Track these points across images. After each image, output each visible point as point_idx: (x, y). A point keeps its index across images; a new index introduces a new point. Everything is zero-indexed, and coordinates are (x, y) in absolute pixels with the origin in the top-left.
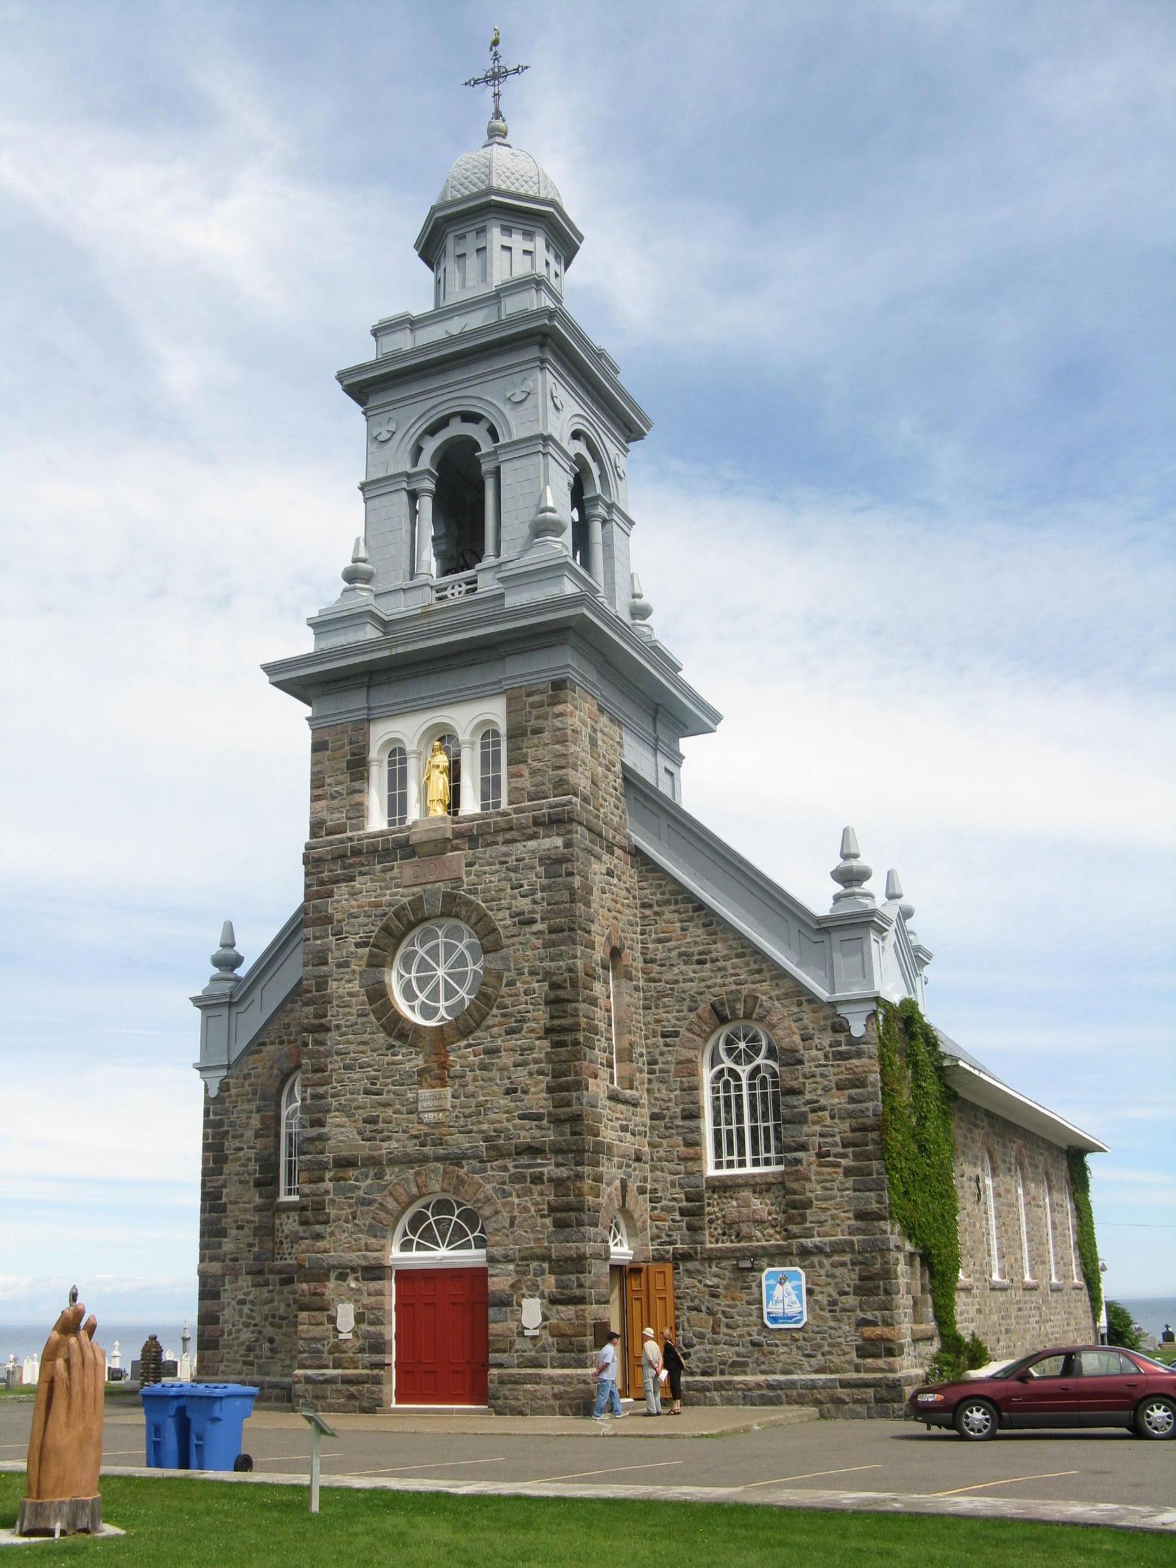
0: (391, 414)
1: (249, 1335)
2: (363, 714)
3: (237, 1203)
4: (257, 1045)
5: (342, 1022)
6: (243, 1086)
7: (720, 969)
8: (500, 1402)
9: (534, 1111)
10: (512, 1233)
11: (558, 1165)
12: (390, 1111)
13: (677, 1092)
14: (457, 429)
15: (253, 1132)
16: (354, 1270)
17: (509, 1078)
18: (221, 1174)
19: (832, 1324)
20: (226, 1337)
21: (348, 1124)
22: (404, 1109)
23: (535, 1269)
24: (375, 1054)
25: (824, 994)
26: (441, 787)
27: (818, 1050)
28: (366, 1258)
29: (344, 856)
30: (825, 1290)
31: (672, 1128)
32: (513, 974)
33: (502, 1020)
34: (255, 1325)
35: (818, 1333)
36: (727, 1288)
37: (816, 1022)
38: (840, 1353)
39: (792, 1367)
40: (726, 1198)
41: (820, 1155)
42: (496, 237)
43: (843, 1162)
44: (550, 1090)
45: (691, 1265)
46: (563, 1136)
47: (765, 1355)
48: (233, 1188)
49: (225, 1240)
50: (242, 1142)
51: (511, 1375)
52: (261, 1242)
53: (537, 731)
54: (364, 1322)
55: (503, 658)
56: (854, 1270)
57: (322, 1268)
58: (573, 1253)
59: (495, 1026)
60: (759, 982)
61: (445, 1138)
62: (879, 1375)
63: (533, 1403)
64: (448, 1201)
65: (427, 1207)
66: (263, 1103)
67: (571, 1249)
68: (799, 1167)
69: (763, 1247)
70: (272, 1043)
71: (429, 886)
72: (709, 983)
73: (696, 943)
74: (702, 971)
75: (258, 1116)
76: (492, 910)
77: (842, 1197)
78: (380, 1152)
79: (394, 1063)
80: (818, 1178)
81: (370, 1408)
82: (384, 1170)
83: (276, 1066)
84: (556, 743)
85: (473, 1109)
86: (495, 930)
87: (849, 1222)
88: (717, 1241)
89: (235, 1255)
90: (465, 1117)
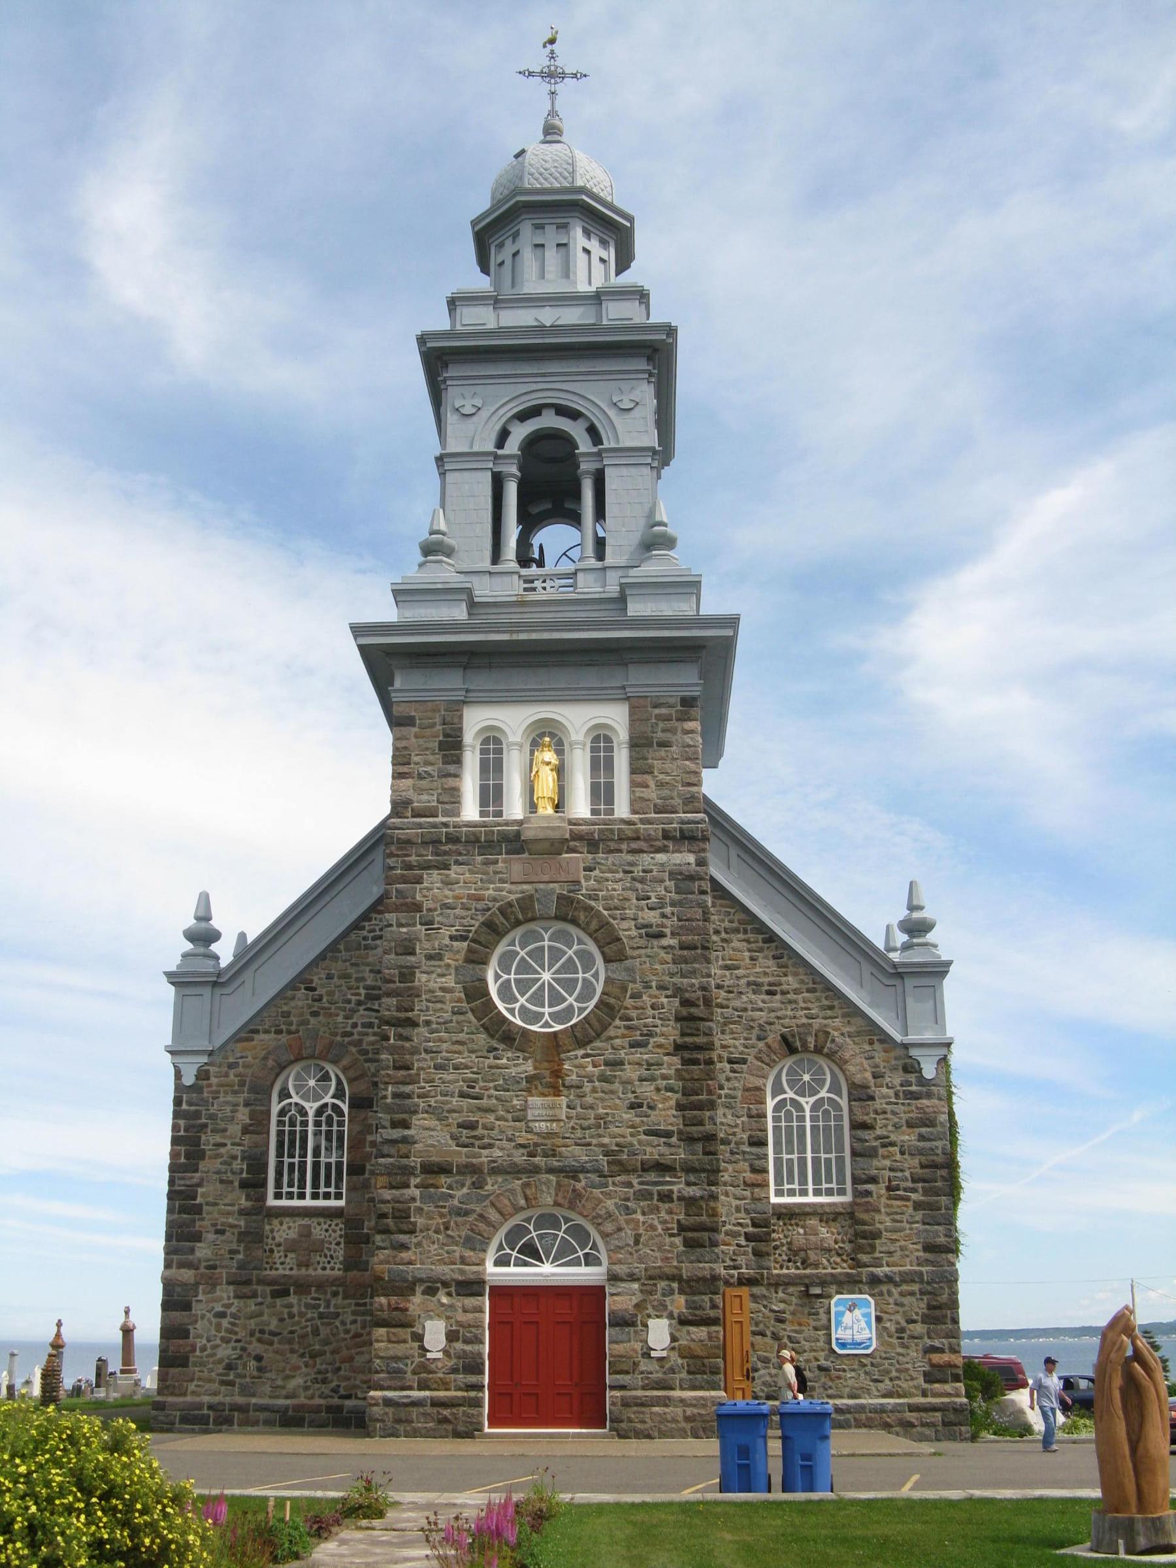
0: (478, 389)
1: (229, 1352)
2: (459, 696)
3: (216, 1204)
4: (248, 1032)
5: (433, 1019)
6: (226, 1075)
7: (790, 1002)
8: (623, 1425)
9: (662, 1128)
10: (637, 1251)
11: (688, 1184)
12: (491, 1118)
13: (745, 1119)
14: (549, 420)
15: (240, 1127)
16: (445, 1284)
17: (634, 1092)
18: (196, 1171)
19: (900, 1350)
20: (198, 1353)
21: (439, 1128)
22: (509, 1116)
23: (663, 1289)
24: (473, 1056)
25: (898, 1037)
26: (551, 784)
27: (888, 1087)
28: (462, 1272)
29: (436, 842)
30: (892, 1317)
31: (738, 1154)
32: (639, 986)
33: (626, 1032)
34: (238, 1341)
35: (887, 1358)
36: (793, 1313)
37: (888, 1062)
38: (908, 1378)
39: (859, 1392)
40: (791, 1225)
41: (889, 1189)
42: (578, 238)
43: (913, 1196)
44: (680, 1107)
45: (757, 1290)
46: (697, 1156)
47: (832, 1380)
48: (211, 1188)
49: (199, 1245)
50: (224, 1138)
51: (636, 1398)
52: (247, 1249)
53: (664, 744)
54: (457, 1340)
55: (626, 665)
56: (922, 1300)
57: (406, 1281)
58: (707, 1274)
59: (617, 1037)
60: (831, 1018)
61: (558, 1149)
62: (946, 1400)
63: (662, 1426)
64: (553, 1215)
65: (528, 1220)
66: (253, 1096)
67: (704, 1269)
68: (869, 1199)
69: (832, 1275)
70: (267, 1032)
71: (542, 886)
72: (779, 1014)
73: (765, 974)
74: (771, 1002)
75: (247, 1110)
76: (615, 919)
77: (911, 1229)
78: (479, 1160)
79: (498, 1067)
80: (888, 1210)
81: (466, 1433)
82: (485, 1179)
83: (271, 1057)
84: (687, 760)
85: (592, 1121)
86: (619, 939)
87: (917, 1254)
88: (781, 1267)
89: (211, 1263)
90: (583, 1129)
